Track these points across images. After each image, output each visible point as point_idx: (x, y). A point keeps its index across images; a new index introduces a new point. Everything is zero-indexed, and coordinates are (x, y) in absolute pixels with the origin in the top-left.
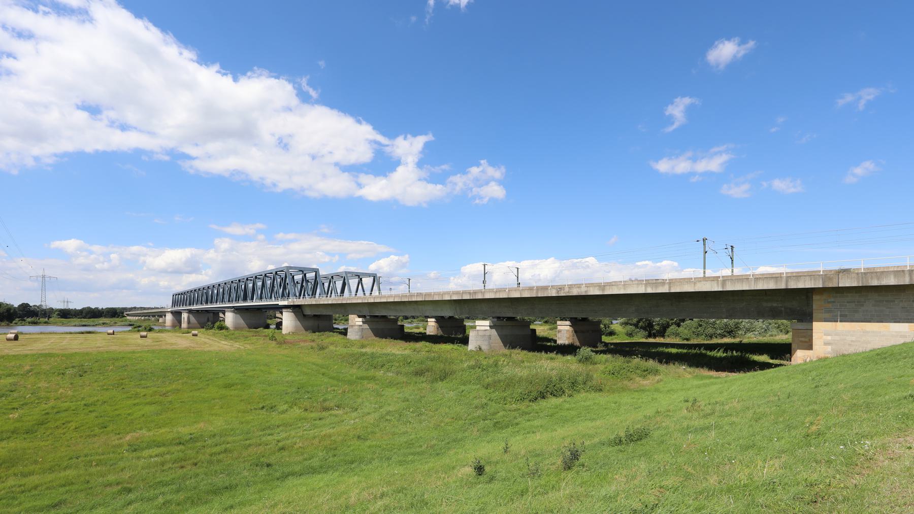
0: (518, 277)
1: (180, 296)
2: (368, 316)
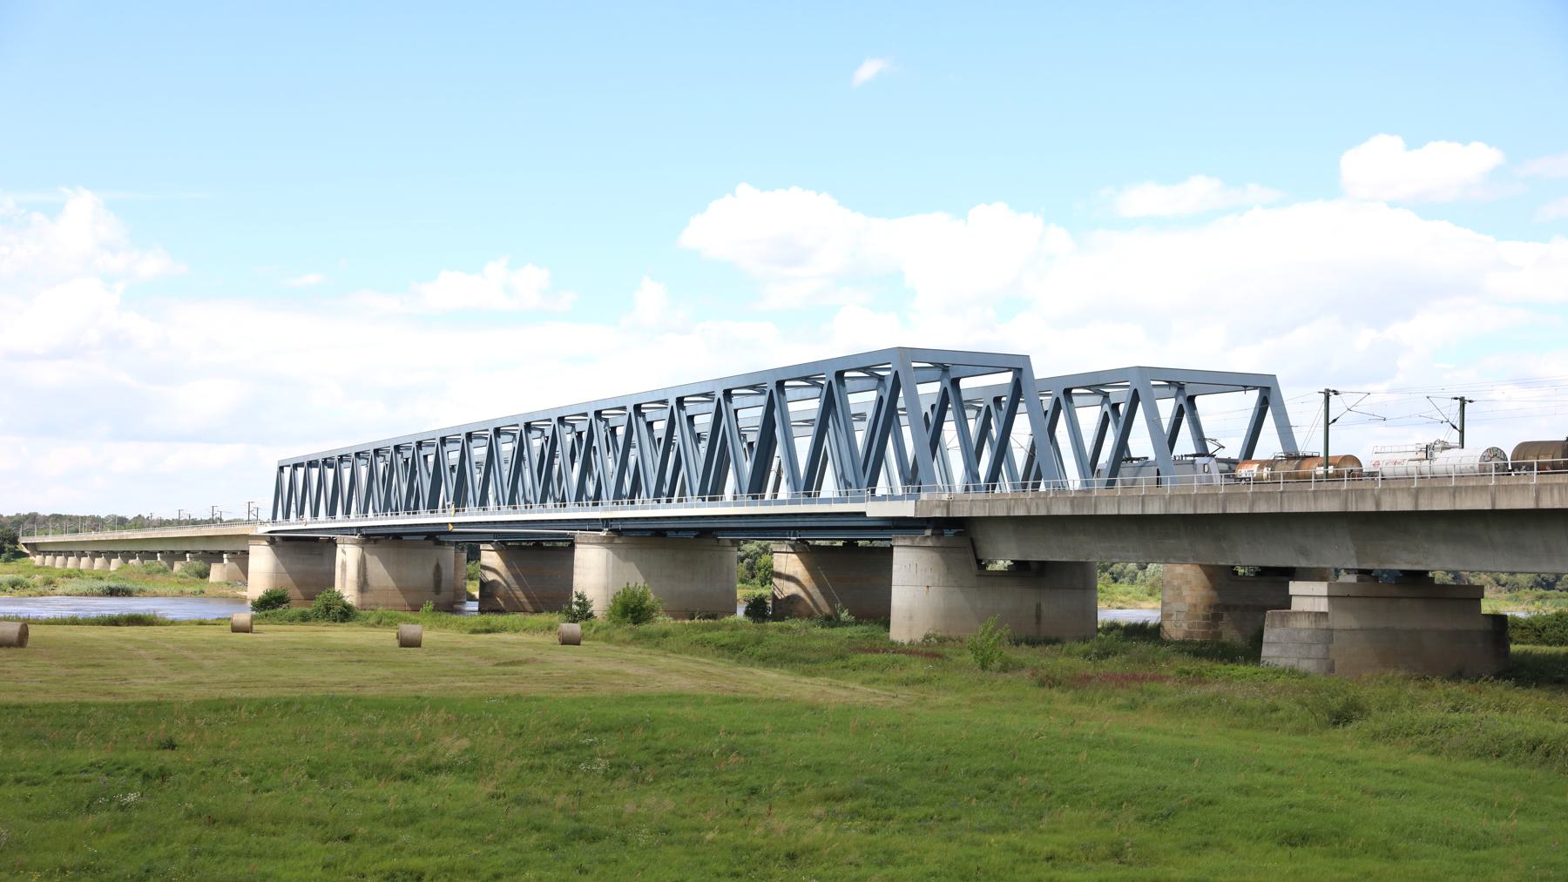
0: (1462, 432)
1: (315, 472)
2: (1348, 571)
